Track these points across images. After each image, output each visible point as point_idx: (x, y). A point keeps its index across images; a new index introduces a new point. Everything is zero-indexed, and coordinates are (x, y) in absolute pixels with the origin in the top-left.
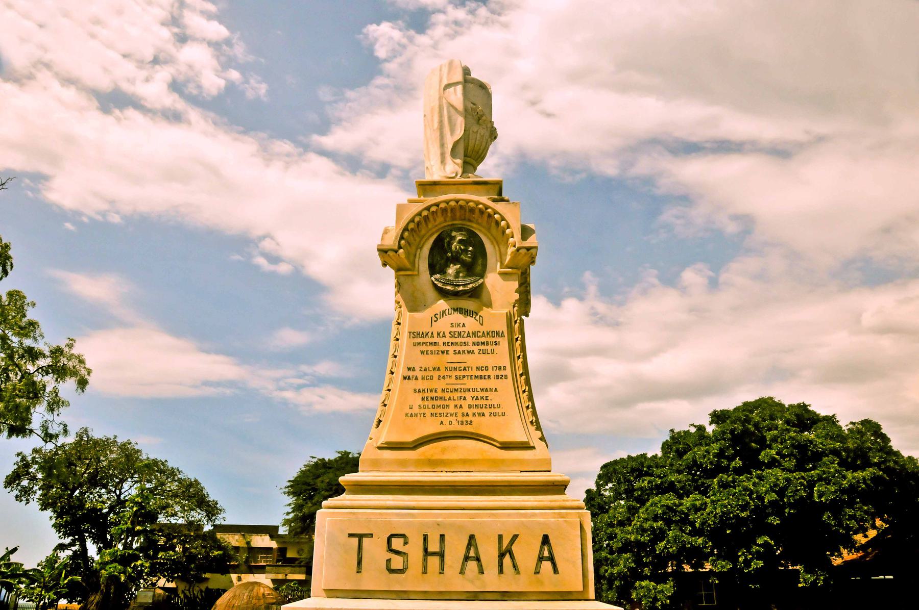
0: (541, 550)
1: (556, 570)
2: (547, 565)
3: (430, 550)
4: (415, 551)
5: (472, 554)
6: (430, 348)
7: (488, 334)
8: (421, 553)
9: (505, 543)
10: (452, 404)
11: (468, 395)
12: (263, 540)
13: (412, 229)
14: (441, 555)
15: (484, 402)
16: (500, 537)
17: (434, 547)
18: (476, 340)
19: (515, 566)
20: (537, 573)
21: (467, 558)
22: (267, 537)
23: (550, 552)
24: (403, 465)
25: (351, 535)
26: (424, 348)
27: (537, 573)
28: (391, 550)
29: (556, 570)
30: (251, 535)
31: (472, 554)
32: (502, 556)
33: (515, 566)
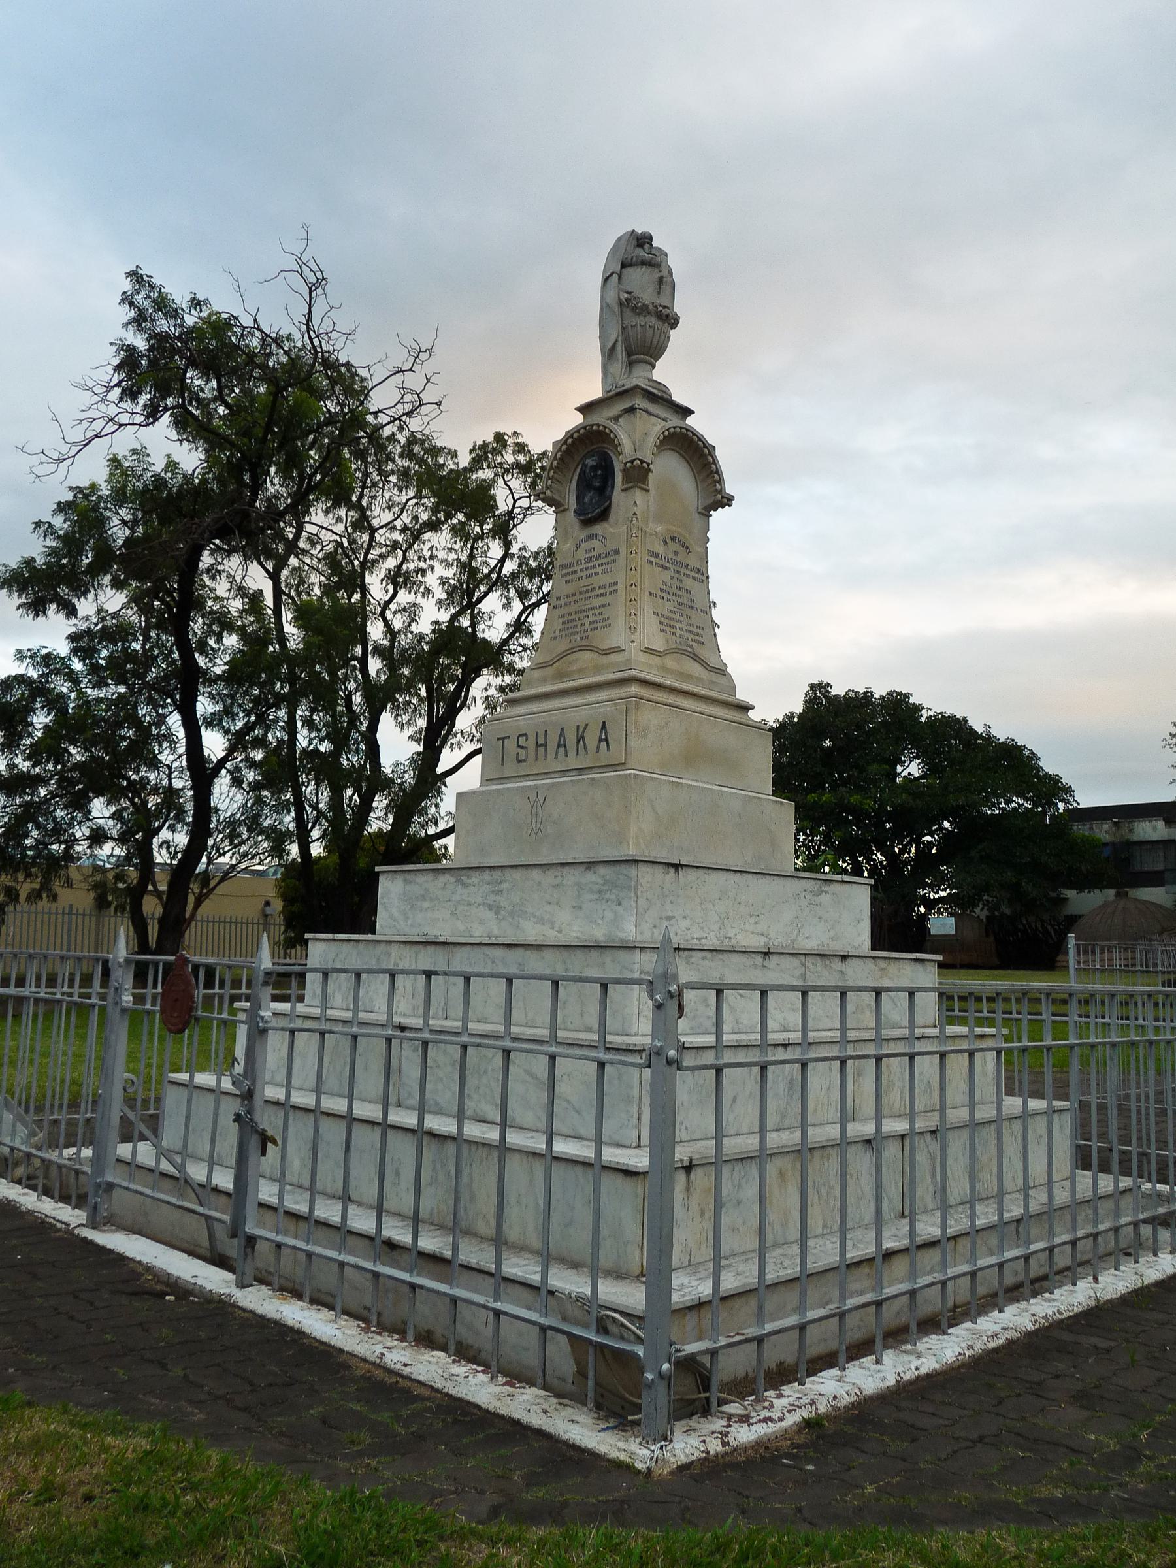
0: (601, 733)
1: (608, 749)
2: (604, 744)
3: (540, 743)
4: (531, 744)
5: (562, 743)
6: (572, 577)
7: (679, 542)
8: (535, 745)
9: (581, 731)
10: (579, 623)
11: (590, 613)
12: (1155, 828)
13: (557, 467)
14: (545, 745)
15: (600, 617)
16: (578, 726)
17: (541, 741)
18: (600, 561)
19: (585, 749)
20: (598, 752)
21: (559, 746)
22: (1161, 824)
23: (606, 735)
24: (544, 680)
25: (499, 739)
26: (567, 578)
27: (598, 752)
28: (519, 746)
29: (608, 749)
30: (1131, 822)
31: (562, 743)
32: (578, 741)
33: (585, 749)
